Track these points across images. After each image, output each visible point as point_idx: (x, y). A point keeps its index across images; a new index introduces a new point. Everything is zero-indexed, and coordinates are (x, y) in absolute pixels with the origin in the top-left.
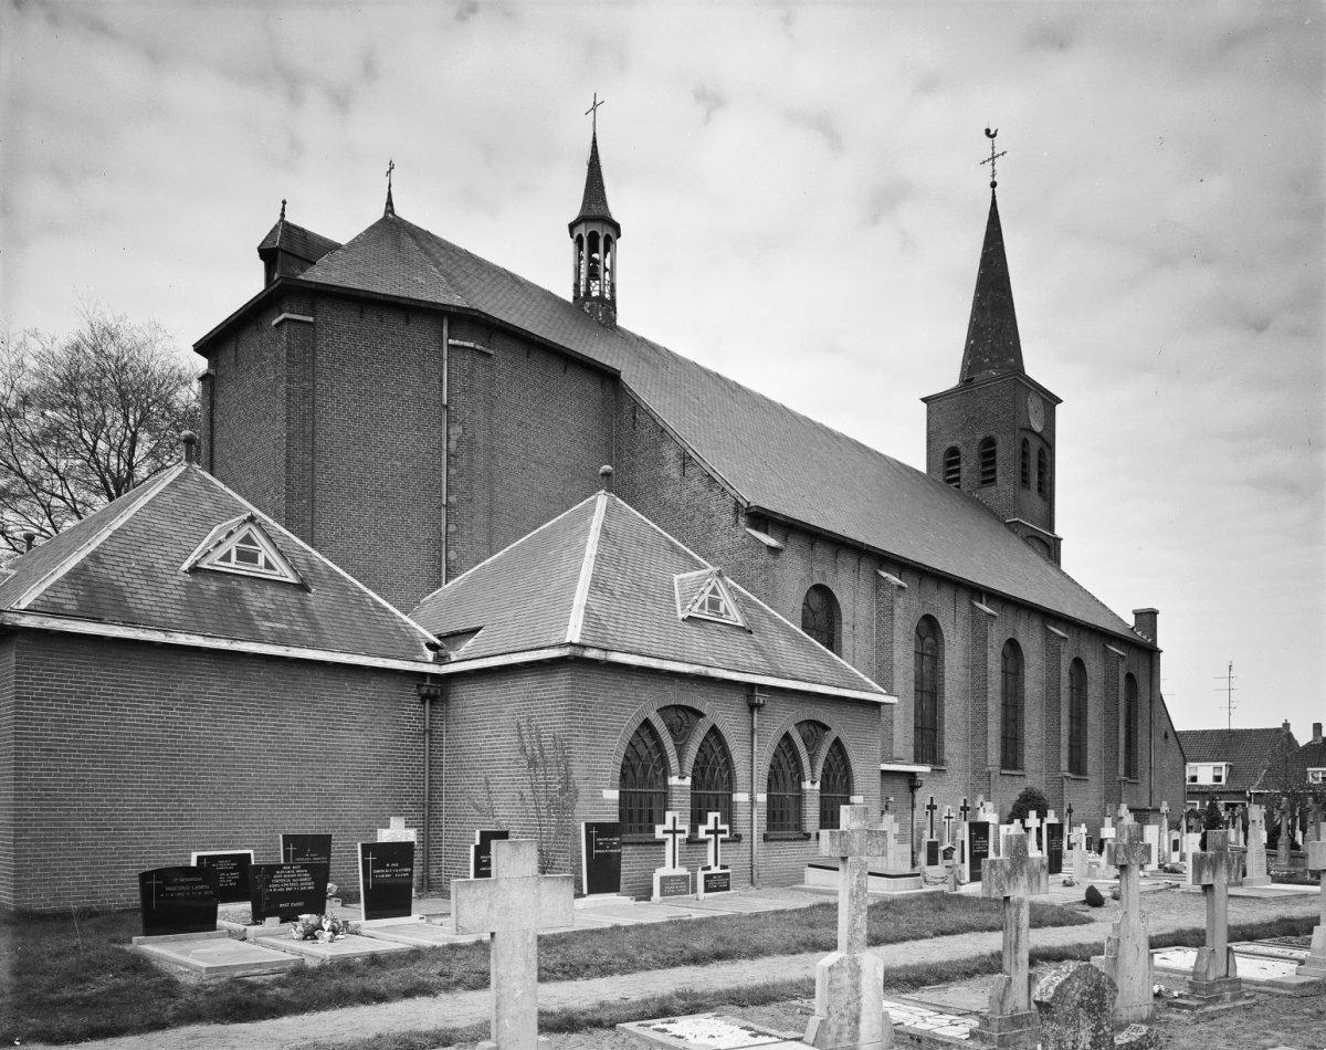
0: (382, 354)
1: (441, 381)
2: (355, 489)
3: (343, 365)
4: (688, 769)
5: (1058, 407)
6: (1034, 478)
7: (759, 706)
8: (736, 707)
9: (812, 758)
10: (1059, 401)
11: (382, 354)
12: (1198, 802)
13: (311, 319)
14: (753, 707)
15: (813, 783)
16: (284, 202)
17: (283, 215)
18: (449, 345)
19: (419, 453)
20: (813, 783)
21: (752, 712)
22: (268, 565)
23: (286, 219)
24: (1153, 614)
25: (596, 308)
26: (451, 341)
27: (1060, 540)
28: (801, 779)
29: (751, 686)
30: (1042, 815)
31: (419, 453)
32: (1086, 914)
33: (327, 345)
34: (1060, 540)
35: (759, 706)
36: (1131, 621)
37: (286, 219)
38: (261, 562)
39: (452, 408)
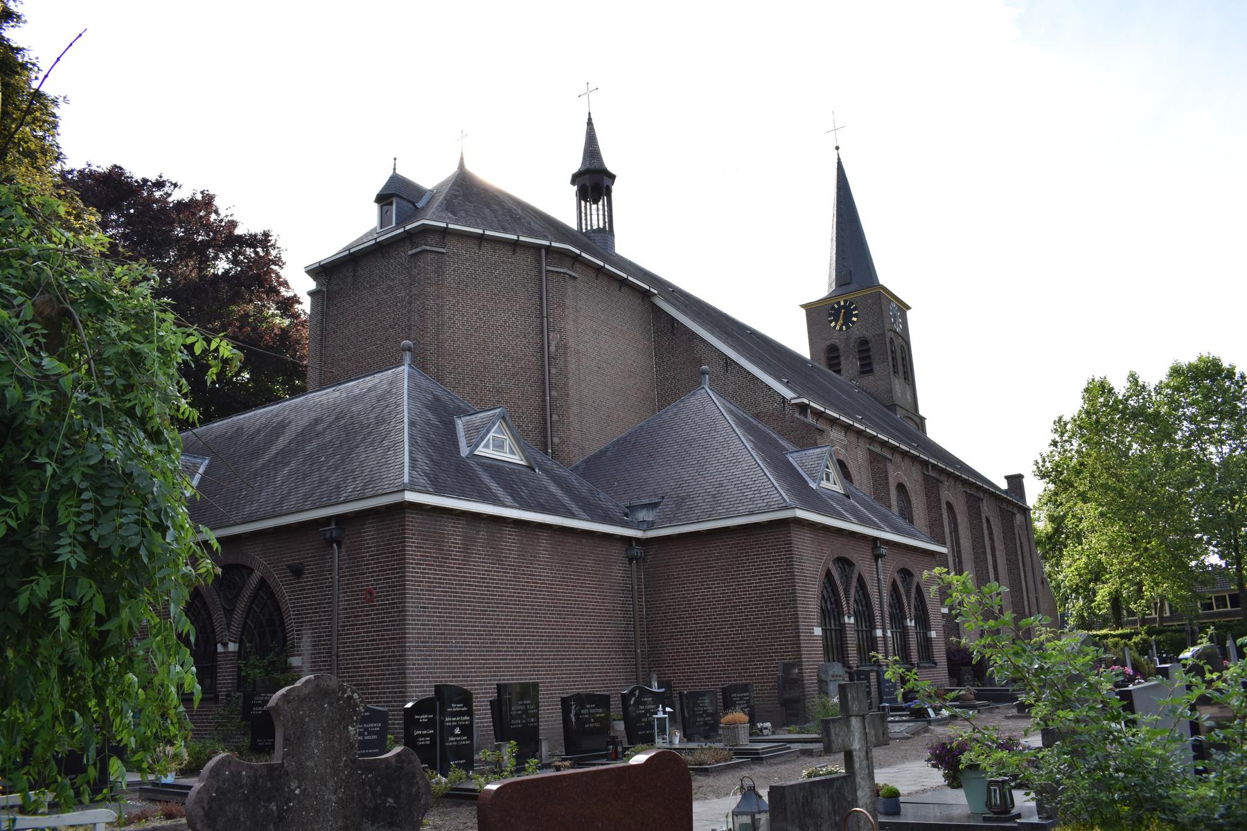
0: (496, 277)
2: (476, 386)
3: (467, 286)
5: (909, 313)
7: (882, 556)
9: (229, 613)
10: (909, 308)
11: (496, 277)
14: (877, 557)
15: (849, 617)
16: (395, 159)
17: (395, 169)
18: (547, 271)
19: (525, 356)
21: (876, 561)
24: (1020, 477)
27: (925, 419)
29: (875, 539)
30: (117, 658)
31: (525, 356)
33: (454, 270)
35: (882, 556)
36: (1003, 485)
39: (551, 320)
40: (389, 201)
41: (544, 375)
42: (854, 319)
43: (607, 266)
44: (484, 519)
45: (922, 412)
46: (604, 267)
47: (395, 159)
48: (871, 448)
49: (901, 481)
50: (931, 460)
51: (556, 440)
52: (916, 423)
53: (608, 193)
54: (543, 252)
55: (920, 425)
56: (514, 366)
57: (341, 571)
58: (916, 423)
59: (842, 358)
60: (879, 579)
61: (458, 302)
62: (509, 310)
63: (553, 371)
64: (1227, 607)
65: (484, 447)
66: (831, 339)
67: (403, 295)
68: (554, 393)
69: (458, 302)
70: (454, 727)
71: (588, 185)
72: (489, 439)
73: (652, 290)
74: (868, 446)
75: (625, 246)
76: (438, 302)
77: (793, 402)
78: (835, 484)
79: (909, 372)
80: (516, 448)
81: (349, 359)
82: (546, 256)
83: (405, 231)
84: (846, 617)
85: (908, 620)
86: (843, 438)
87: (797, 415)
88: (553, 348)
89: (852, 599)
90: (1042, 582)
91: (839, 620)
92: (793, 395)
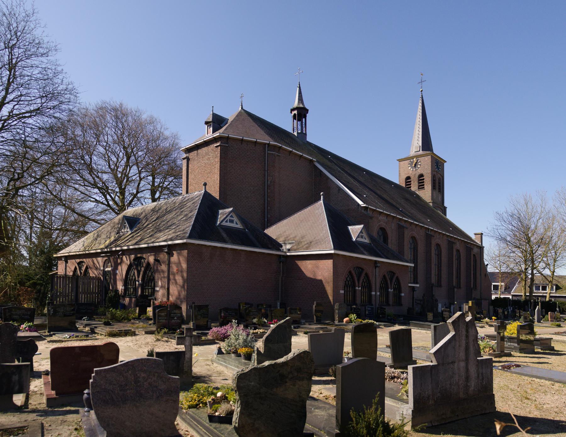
0: (248, 155)
1: (265, 164)
4: (360, 285)
5: (445, 164)
6: (437, 182)
8: (90, 108)
11: (248, 155)
12: (493, 284)
13: (227, 145)
15: (391, 289)
20: (391, 289)
21: (376, 268)
22: (236, 224)
23: (214, 112)
25: (303, 135)
26: (269, 152)
27: (446, 208)
28: (388, 288)
32: (195, 195)
34: (446, 208)
37: (214, 112)
38: (235, 222)
39: (269, 172)
40: (210, 124)
41: (265, 192)
42: (410, 168)
43: (293, 151)
44: (218, 248)
45: (445, 205)
46: (292, 151)
47: (213, 107)
48: (399, 223)
49: (413, 235)
50: (430, 228)
51: (269, 216)
52: (441, 209)
53: (305, 117)
54: (267, 145)
55: (443, 210)
56: (253, 189)
57: (392, 244)
58: (441, 209)
59: (412, 182)
60: (376, 275)
61: (233, 165)
62: (252, 168)
63: (269, 191)
64: (540, 290)
65: (225, 222)
66: (408, 174)
67: (213, 161)
68: (269, 199)
69: (233, 165)
70: (175, 317)
71: (296, 114)
72: (227, 220)
73: (314, 159)
74: (398, 222)
75: (310, 139)
76: (224, 165)
77: (362, 206)
78: (365, 239)
79: (442, 189)
80: (238, 222)
81: (196, 184)
82: (268, 147)
83: (213, 137)
84: (390, 289)
85: (390, 289)
86: (385, 219)
87: (363, 211)
88: (269, 182)
89: (361, 282)
90: (485, 275)
91: (354, 288)
92: (363, 203)
